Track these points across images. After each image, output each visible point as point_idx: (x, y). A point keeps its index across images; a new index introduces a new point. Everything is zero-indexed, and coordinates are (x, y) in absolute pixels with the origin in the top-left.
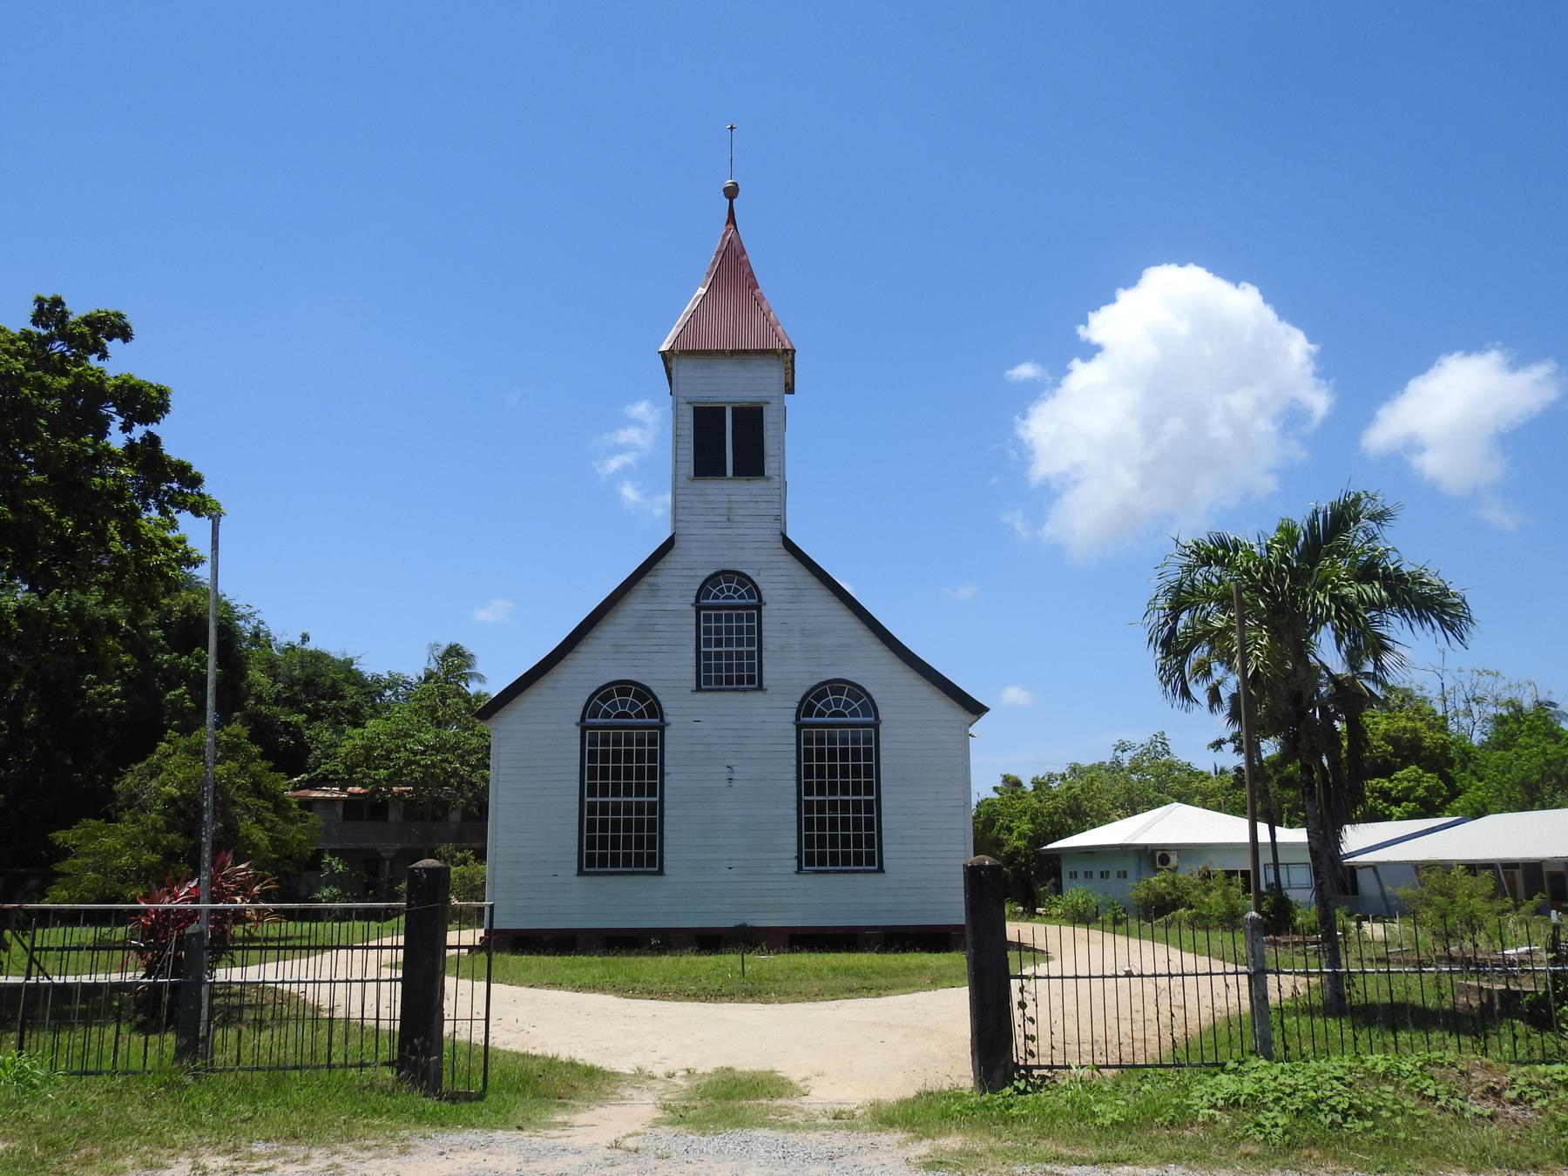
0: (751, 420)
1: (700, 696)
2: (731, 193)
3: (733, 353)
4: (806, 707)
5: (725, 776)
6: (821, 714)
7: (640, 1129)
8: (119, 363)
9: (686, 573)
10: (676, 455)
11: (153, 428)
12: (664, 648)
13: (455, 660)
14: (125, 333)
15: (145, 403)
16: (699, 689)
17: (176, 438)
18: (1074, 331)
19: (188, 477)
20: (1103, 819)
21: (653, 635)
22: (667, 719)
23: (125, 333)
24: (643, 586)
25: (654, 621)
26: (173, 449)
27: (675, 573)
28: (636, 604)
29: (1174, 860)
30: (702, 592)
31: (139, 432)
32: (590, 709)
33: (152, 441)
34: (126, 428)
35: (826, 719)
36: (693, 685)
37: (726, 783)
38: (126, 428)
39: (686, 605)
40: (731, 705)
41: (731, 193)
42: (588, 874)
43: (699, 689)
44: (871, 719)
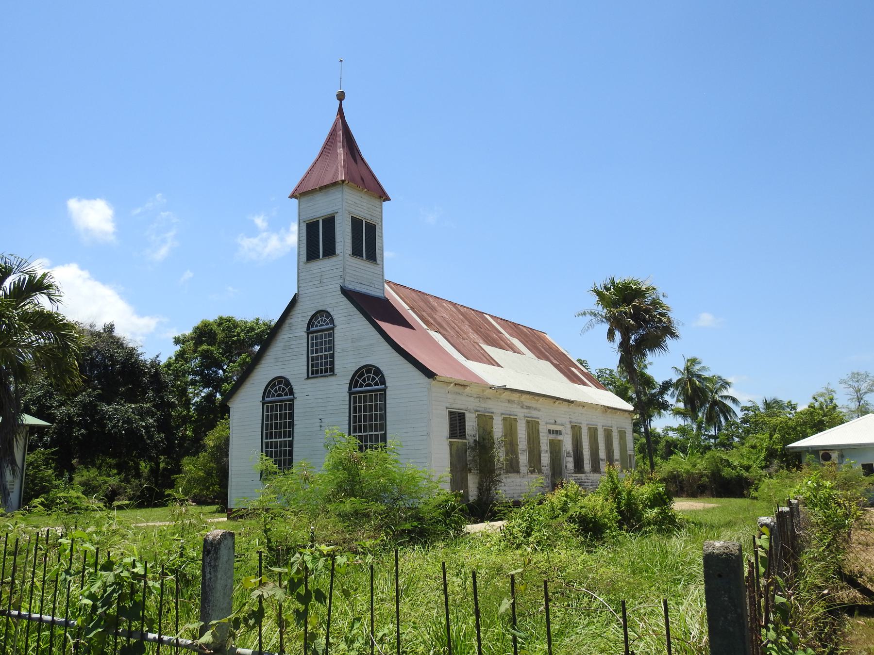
1: (310, 381)
2: (341, 97)
3: (321, 188)
4: (354, 382)
5: (319, 425)
6: (361, 386)
9: (303, 315)
10: (299, 252)
12: (295, 357)
16: (308, 378)
18: (65, 207)
20: (805, 436)
21: (290, 351)
22: (296, 395)
25: (291, 343)
27: (299, 315)
29: (835, 455)
30: (310, 324)
32: (266, 393)
35: (363, 389)
36: (306, 376)
37: (319, 428)
40: (321, 383)
41: (341, 97)
43: (308, 378)
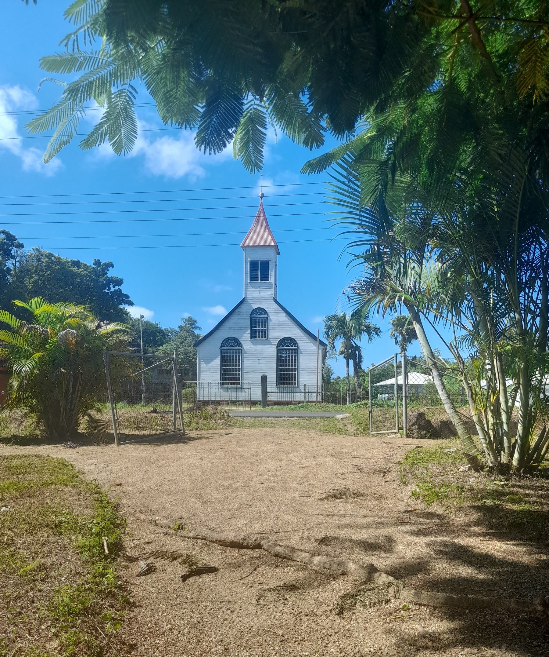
0: (265, 265)
7: (353, 482)
8: (111, 273)
11: (120, 287)
13: (191, 322)
14: (112, 266)
15: (119, 282)
17: (124, 289)
19: (127, 297)
23: (112, 266)
24: (236, 311)
26: (124, 292)
28: (235, 317)
31: (117, 288)
32: (222, 345)
33: (120, 290)
34: (114, 287)
38: (114, 287)
39: (248, 317)
42: (121, 444)
44: (296, 348)
